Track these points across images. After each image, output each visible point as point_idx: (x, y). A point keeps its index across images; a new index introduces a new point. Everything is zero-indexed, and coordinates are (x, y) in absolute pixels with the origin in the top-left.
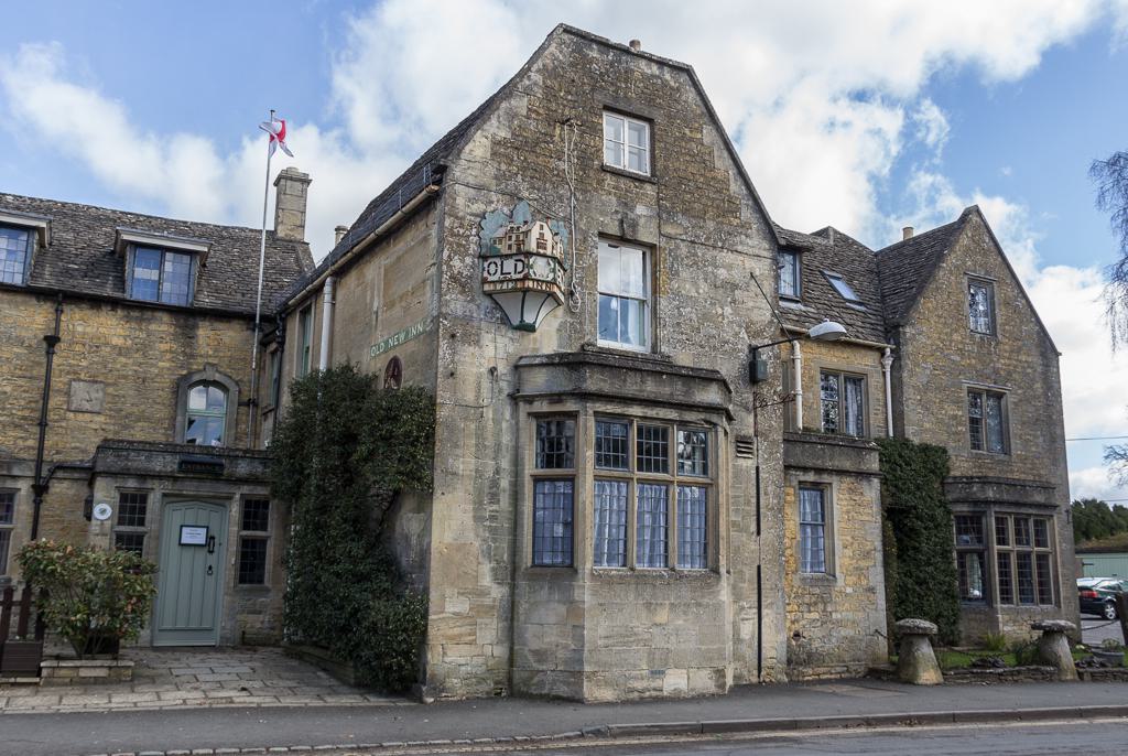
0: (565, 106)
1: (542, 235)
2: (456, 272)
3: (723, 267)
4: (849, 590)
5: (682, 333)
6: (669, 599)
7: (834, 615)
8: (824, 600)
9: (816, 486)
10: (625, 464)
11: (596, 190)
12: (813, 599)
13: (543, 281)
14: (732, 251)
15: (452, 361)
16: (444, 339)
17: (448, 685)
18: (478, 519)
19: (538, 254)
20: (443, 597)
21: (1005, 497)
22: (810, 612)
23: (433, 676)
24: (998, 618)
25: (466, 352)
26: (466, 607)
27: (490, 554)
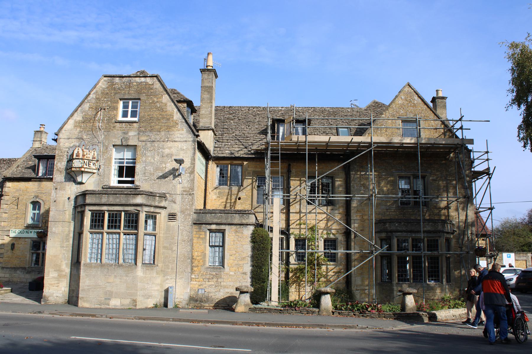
0: (103, 103)
1: (78, 152)
3: (167, 148)
4: (232, 273)
5: (146, 176)
6: (114, 274)
7: (222, 283)
8: (218, 276)
9: (219, 231)
10: (119, 228)
11: (112, 130)
12: (211, 276)
13: (77, 168)
14: (172, 141)
15: (56, 197)
17: (49, 299)
19: (76, 159)
20: (49, 272)
21: (404, 229)
22: (209, 281)
23: (45, 296)
24: (393, 289)
25: (60, 193)
26: (57, 275)
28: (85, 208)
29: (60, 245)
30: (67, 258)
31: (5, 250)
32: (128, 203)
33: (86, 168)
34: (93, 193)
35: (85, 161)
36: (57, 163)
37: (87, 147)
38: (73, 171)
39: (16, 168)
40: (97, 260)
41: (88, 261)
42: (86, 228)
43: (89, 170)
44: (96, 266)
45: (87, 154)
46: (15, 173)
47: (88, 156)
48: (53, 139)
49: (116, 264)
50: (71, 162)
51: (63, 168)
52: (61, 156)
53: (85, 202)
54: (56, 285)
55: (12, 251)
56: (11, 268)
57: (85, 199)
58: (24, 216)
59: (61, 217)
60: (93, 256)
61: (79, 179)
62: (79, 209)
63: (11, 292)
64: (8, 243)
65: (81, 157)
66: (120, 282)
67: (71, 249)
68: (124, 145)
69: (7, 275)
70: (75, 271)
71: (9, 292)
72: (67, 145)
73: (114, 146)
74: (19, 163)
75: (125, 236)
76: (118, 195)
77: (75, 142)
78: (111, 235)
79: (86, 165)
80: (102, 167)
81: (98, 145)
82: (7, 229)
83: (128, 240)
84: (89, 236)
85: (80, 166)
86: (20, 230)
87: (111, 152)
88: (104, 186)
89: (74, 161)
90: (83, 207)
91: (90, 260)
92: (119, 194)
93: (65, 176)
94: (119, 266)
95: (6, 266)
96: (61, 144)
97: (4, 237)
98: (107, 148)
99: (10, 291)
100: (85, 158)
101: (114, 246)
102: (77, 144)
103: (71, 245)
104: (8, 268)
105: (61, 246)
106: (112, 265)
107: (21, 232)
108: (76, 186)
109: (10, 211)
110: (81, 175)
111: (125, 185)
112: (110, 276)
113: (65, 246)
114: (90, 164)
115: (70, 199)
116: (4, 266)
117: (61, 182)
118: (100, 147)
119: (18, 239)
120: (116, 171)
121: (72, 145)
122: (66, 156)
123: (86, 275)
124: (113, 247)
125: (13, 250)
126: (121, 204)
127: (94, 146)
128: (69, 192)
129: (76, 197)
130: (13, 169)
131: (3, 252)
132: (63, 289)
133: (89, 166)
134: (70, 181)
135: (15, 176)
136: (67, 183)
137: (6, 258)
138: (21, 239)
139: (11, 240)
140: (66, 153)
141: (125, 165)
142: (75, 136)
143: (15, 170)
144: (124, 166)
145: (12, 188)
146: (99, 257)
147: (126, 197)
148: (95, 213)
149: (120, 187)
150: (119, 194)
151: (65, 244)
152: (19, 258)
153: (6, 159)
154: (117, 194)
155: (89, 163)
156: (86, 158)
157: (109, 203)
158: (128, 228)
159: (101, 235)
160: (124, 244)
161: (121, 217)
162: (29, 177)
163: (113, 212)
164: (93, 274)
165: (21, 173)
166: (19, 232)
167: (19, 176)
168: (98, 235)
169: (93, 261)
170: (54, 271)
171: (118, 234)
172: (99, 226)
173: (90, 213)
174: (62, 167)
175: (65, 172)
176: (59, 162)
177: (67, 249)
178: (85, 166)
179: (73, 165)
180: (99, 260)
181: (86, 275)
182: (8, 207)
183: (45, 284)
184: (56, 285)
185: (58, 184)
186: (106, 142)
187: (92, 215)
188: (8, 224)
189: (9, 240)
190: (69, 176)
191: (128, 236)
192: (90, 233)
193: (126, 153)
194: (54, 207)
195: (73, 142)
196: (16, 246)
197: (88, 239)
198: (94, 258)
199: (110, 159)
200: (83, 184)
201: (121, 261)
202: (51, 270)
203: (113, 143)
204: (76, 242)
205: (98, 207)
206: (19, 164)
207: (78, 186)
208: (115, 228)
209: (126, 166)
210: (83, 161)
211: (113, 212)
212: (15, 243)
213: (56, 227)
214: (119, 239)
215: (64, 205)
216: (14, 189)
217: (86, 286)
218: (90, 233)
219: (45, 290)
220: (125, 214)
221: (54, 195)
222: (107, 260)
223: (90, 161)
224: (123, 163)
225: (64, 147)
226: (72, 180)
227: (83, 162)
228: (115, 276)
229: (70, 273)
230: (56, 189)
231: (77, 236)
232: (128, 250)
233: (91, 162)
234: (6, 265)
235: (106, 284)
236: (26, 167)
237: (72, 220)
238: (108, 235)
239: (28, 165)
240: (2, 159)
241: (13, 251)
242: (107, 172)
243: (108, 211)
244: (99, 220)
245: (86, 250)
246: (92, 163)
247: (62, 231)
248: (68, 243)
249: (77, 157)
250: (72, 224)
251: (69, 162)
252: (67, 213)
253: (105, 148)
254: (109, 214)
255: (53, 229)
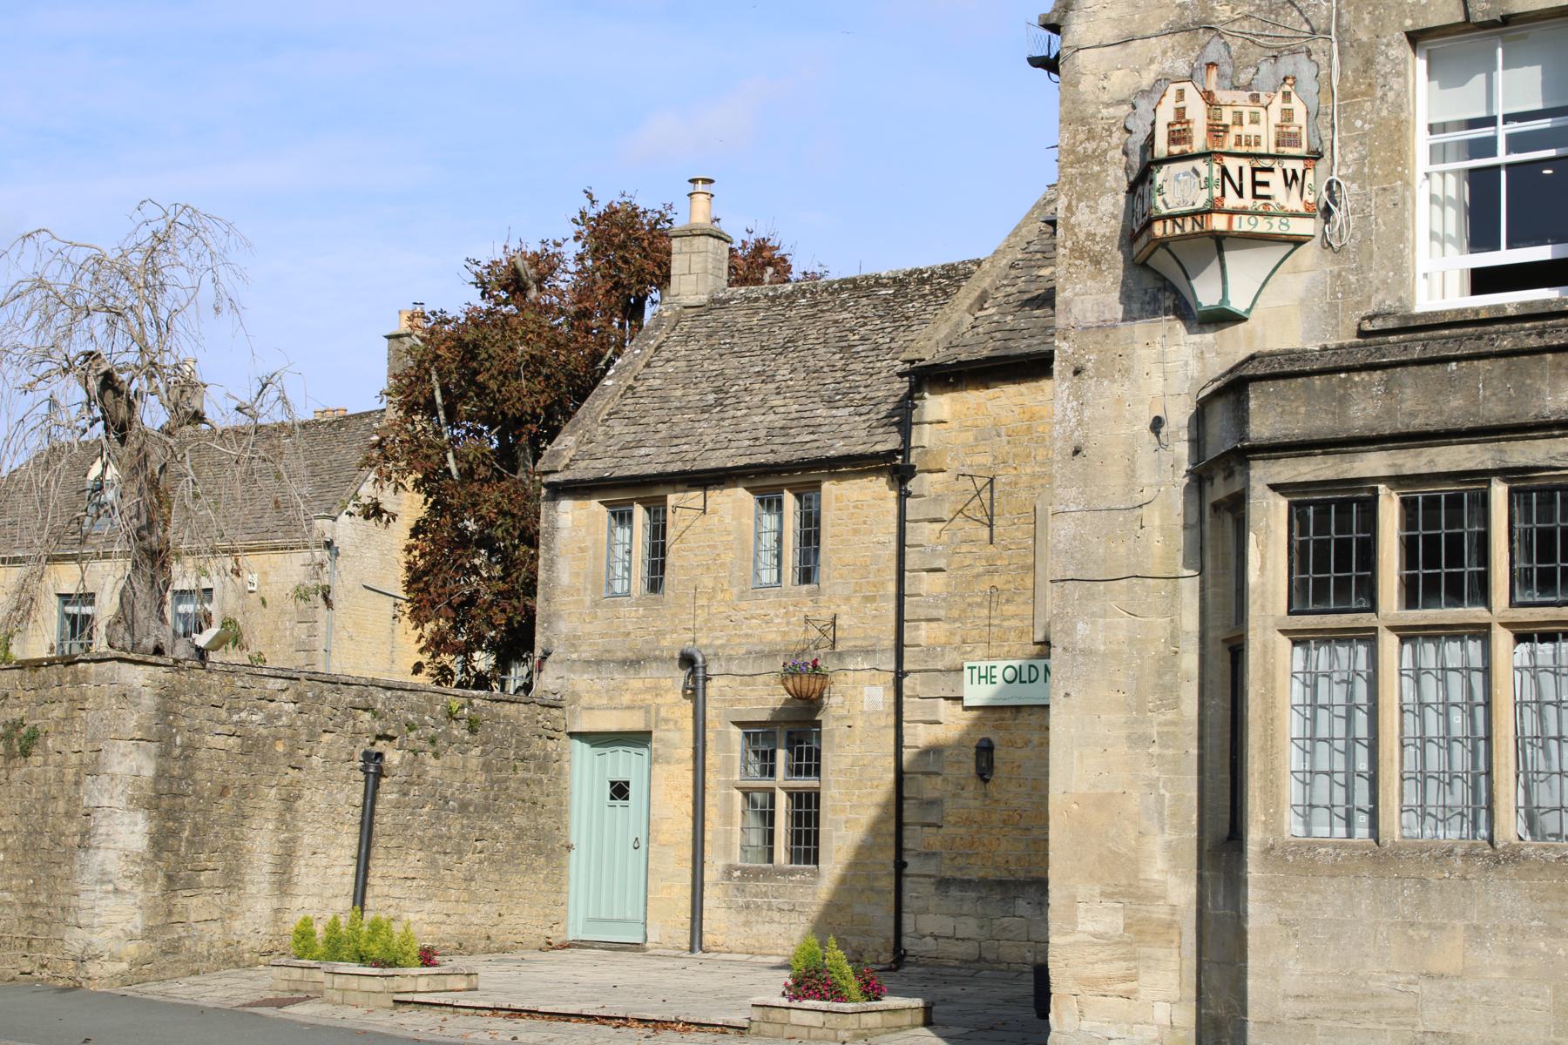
1: (1180, 112)
2: (1082, 237)
6: (1463, 915)
10: (1482, 592)
13: (1183, 215)
15: (1080, 423)
16: (1063, 380)
18: (1138, 741)
19: (1171, 159)
20: (1073, 901)
27: (1161, 814)
28: (1248, 479)
29: (1124, 732)
30: (1173, 815)
31: (945, 780)
32: (1529, 417)
33: (1243, 211)
34: (1287, 368)
35: (1232, 165)
36: (1069, 208)
37: (1244, 78)
38: (1164, 243)
39: (970, 310)
40: (1349, 821)
41: (1293, 826)
42: (1263, 607)
43: (1262, 226)
44: (1343, 863)
45: (1239, 121)
46: (968, 336)
47: (1248, 129)
48: (1036, 62)
49: (1472, 847)
50: (1147, 185)
51: (1107, 232)
52: (1087, 158)
53: (1243, 437)
54: (1122, 987)
55: (980, 783)
56: (984, 883)
57: (1241, 418)
58: (1029, 582)
59: (1122, 550)
60: (1321, 794)
61: (1206, 293)
62: (1219, 490)
63: (928, 1023)
64: (960, 744)
65: (1199, 143)
66: (1513, 971)
67: (1194, 752)
68: (1478, 17)
69: (969, 927)
70: (1220, 899)
71: (914, 1026)
72: (1120, 82)
73: (1415, 38)
74: (988, 280)
75: (1524, 648)
76: (1453, 365)
77: (1164, 53)
78: (1430, 647)
79: (1240, 194)
80: (1349, 190)
81: (1309, 53)
82: (950, 659)
83: (1547, 680)
84: (1288, 658)
85: (1199, 205)
86: (1016, 663)
87: (1396, 83)
88: (1371, 318)
89: (1159, 177)
90: (1238, 468)
91: (1307, 824)
92: (1458, 359)
93: (1124, 283)
94: (1501, 858)
95: (958, 875)
96: (1087, 85)
97: (935, 708)
98: (1369, 62)
99: (920, 1018)
100: (1229, 144)
101: (1457, 717)
102: (1182, 68)
103: (1194, 729)
104: (969, 882)
105: (1128, 737)
106: (1450, 852)
107: (1018, 673)
108: (1196, 338)
109: (957, 558)
110: (1215, 266)
111: (1510, 300)
112: (1442, 927)
113: (1154, 732)
114: (1266, 184)
115: (1163, 430)
116: (949, 874)
117: (1103, 327)
118: (1323, 60)
119: (1008, 714)
120: (1451, 213)
121: (1147, 79)
122: (1117, 154)
123: (1285, 923)
124: (1448, 727)
125: (986, 781)
126: (1481, 422)
127: (1282, 60)
128: (1157, 384)
129: (1200, 418)
130: (955, 317)
131: (936, 794)
132: (1162, 1013)
133: (1255, 196)
134: (1155, 314)
135: (963, 357)
136: (1140, 328)
137: (955, 824)
138: (1024, 714)
139: (976, 724)
140: (1117, 137)
141: (1502, 157)
142: (1162, 18)
143: (969, 319)
144: (1497, 168)
145: (954, 424)
146: (1362, 798)
147: (1508, 373)
148: (1314, 503)
149: (1476, 311)
150: (1458, 359)
151: (1156, 723)
152: (1023, 824)
153: (933, 272)
154: (1446, 360)
155: (1260, 177)
156: (1238, 143)
157: (1400, 425)
158: (1542, 592)
159: (1362, 650)
160: (1520, 704)
161: (1485, 519)
162: (1033, 349)
163: (1430, 489)
164: (1329, 914)
165: (998, 335)
166: (1010, 674)
167: (985, 353)
168: (1343, 651)
169: (1321, 831)
170: (1103, 894)
171: (1473, 637)
172: (1343, 585)
173: (1283, 503)
174: (1102, 230)
175: (1120, 256)
176: (1079, 200)
177: (1170, 752)
178: (1231, 200)
179: (1158, 201)
180: (1362, 819)
181: (1285, 923)
182: (945, 537)
183: (1053, 979)
184: (1122, 987)
185: (1089, 339)
186: (1358, 20)
187: (1297, 512)
188: (953, 634)
189: (964, 723)
190: (1148, 282)
191: (1547, 647)
192: (1295, 643)
193: (1500, 75)
194: (1073, 492)
195: (1152, 61)
196: (999, 754)
197: (1282, 678)
198: (1331, 807)
199: (1394, 134)
200: (1235, 318)
201: (1510, 826)
202: (1082, 890)
203: (1408, 23)
204: (1221, 704)
205: (1330, 460)
206: (986, 283)
207: (1209, 337)
208: (1456, 598)
209: (1509, 166)
210: (1216, 167)
211: (1430, 489)
212: (995, 738)
213: (1093, 614)
214: (1487, 671)
215: (1131, 473)
216: (967, 429)
217: (1286, 997)
218: (1295, 643)
219: (1058, 1017)
220: (1511, 492)
221: (1070, 413)
222: (1410, 818)
223: (1267, 163)
224: (1488, 147)
225: (1105, 97)
226: (1169, 303)
227: (1217, 175)
228: (1476, 934)
229: (1194, 908)
230: (1077, 372)
231: (1222, 664)
232: (1553, 744)
233: (1271, 170)
234: (960, 869)
235: (1416, 989)
236: (1026, 297)
237: (1186, 565)
238: (1407, 647)
239: (1033, 287)
240: (911, 274)
241: (990, 786)
242: (1381, 226)
243: (1396, 481)
244: (1343, 546)
245: (1270, 751)
246: (1279, 173)
247: (1131, 642)
248: (1170, 715)
249: (1176, 150)
250: (1189, 590)
251: (1140, 190)
252: (1153, 517)
253: (1355, 62)
254: (1408, 505)
255: (1080, 626)
